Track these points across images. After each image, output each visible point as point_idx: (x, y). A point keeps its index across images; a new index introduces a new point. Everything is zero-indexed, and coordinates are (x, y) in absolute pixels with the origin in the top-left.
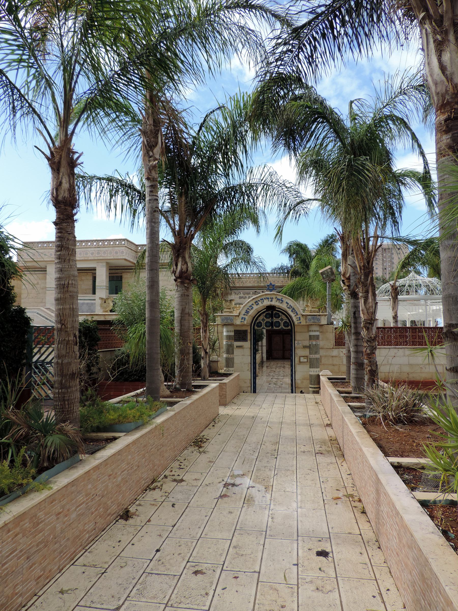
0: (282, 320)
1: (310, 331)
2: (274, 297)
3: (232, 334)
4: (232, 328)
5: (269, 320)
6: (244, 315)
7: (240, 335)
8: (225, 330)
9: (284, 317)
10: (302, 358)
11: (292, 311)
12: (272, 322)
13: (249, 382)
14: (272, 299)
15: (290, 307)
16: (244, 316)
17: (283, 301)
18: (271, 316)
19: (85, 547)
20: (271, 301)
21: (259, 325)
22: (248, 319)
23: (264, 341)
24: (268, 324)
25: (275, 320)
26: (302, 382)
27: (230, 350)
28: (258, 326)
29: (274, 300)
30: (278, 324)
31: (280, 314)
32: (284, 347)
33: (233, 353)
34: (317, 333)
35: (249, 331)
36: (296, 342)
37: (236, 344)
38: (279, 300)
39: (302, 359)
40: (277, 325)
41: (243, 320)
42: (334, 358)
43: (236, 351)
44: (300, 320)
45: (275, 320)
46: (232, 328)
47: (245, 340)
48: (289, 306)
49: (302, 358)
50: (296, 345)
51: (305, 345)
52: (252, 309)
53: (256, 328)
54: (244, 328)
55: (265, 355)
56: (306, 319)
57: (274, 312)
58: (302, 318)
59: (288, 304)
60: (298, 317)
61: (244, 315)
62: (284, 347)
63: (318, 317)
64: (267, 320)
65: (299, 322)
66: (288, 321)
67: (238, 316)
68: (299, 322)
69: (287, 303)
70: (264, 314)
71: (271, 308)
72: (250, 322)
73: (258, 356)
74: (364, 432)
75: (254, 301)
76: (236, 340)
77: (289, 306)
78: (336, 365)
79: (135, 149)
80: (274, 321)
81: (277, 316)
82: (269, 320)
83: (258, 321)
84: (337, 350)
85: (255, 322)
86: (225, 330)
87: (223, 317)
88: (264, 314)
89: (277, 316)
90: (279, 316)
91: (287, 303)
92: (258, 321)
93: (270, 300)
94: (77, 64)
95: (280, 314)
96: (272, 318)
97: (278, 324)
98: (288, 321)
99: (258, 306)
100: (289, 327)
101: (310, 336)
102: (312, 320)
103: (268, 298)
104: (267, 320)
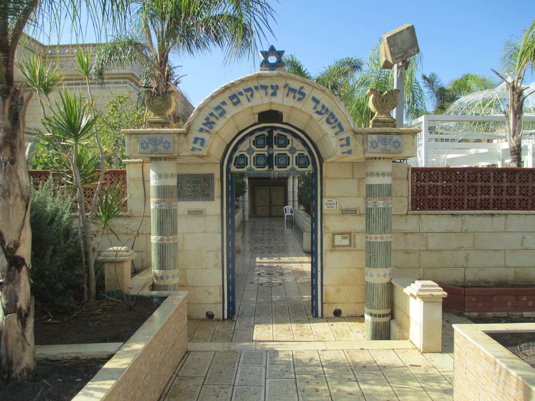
1: (372, 174)
2: (281, 83)
3: (173, 182)
5: (264, 151)
6: (201, 130)
7: (193, 186)
8: (152, 174)
9: (296, 144)
10: (338, 238)
11: (328, 121)
12: (271, 156)
13: (218, 291)
14: (275, 88)
15: (323, 111)
17: (303, 94)
18: (269, 141)
20: (274, 94)
21: (241, 161)
22: (215, 147)
23: (247, 195)
24: (262, 161)
25: (276, 150)
26: (338, 291)
27: (167, 222)
28: (238, 166)
29: (281, 93)
30: (285, 161)
31: (289, 137)
32: (270, 202)
33: (175, 232)
34: (387, 180)
35: (217, 176)
36: (325, 201)
37: (183, 207)
38: (293, 90)
39: (339, 240)
40: (283, 162)
41: (198, 146)
42: (409, 236)
43: (183, 225)
44: (348, 144)
45: (276, 150)
46: (171, 168)
47: (208, 196)
48: (319, 108)
49: (338, 238)
50: (325, 207)
51: (344, 206)
52: (221, 115)
53: (233, 169)
54: (205, 170)
55: (247, 213)
56: (364, 142)
57: (275, 133)
58: (353, 142)
60: (344, 136)
61: (201, 130)
62: (270, 202)
63: (395, 137)
65: (346, 149)
66: (306, 153)
67: (186, 134)
68: (346, 149)
69: (314, 99)
70: (253, 138)
71: (271, 116)
73: (238, 217)
75: (228, 94)
76: (181, 196)
77: (319, 108)
78: (414, 252)
79: (118, 10)
80: (276, 153)
81: (282, 142)
82: (264, 151)
83: (237, 154)
84: (415, 219)
86: (152, 174)
87: (145, 138)
88: (253, 138)
89: (282, 142)
90: (287, 142)
91: (314, 99)
92: (237, 154)
93: (270, 91)
95: (289, 137)
96: (271, 146)
99: (238, 109)
100: (310, 168)
101: (370, 188)
102: (381, 146)
103: (265, 88)
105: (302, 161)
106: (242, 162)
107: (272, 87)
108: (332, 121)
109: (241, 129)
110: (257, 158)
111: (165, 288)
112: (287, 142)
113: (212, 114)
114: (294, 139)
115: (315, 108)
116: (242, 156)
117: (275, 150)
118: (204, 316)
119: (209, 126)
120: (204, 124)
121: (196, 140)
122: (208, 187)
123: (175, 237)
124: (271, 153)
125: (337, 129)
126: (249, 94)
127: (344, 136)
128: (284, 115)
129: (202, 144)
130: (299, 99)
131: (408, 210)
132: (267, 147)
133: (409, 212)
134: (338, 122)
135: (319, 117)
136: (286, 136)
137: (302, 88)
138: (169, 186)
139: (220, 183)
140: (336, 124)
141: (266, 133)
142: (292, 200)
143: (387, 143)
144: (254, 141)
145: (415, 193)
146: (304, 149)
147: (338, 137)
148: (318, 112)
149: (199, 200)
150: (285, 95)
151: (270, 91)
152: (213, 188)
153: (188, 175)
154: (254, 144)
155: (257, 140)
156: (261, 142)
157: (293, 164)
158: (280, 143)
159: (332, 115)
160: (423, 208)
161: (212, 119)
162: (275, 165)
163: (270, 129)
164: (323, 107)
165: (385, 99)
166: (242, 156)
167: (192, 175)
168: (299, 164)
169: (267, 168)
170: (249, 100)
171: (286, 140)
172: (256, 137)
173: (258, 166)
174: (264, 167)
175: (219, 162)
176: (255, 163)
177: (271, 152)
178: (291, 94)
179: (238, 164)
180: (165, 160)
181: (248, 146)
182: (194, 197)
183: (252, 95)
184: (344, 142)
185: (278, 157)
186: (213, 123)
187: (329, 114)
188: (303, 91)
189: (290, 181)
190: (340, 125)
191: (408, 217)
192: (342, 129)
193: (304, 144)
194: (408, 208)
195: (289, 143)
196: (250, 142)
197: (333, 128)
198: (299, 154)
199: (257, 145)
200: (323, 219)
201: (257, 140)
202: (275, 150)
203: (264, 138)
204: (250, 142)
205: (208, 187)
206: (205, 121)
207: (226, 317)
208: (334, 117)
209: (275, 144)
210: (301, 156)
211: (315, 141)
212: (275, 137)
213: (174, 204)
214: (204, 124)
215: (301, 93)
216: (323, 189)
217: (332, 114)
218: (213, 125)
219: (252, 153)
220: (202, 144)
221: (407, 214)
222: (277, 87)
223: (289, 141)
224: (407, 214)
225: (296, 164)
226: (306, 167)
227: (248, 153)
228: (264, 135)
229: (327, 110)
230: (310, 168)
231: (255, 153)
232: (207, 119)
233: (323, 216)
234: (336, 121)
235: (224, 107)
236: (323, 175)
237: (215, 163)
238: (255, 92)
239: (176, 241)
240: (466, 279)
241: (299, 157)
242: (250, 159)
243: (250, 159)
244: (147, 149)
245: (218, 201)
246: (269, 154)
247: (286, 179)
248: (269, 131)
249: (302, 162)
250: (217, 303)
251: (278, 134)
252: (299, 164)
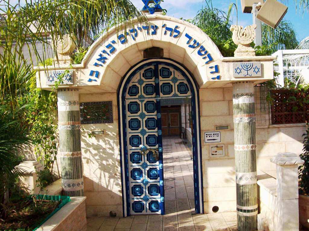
0: (175, 80)
4: (75, 97)
5: (152, 81)
9: (178, 75)
11: (199, 53)
12: (157, 85)
16: (95, 69)
18: (155, 73)
19: (86, 207)
20: (154, 33)
24: (150, 90)
25: (162, 81)
31: (172, 70)
35: (115, 103)
38: (170, 29)
41: (93, 78)
45: (162, 81)
47: (109, 120)
48: (192, 43)
54: (105, 99)
57: (160, 67)
59: (190, 38)
61: (96, 65)
64: (147, 81)
65: (216, 75)
66: (186, 82)
68: (216, 75)
69: (187, 35)
70: (142, 71)
72: (116, 87)
74: (258, 219)
76: (86, 121)
77: (192, 43)
81: (166, 73)
82: (152, 81)
83: (130, 85)
85: (126, 86)
88: (142, 71)
89: (166, 73)
90: (170, 74)
91: (187, 35)
92: (130, 85)
94: (11, 11)
95: (172, 70)
96: (157, 77)
97: (168, 89)
98: (186, 82)
99: (127, 45)
100: (189, 93)
104: (147, 81)
105: (183, 88)
106: (134, 91)
107: (153, 27)
108: (203, 53)
109: (133, 64)
110: (146, 87)
111: (72, 194)
112: (170, 74)
113: (104, 52)
114: (176, 71)
115: (188, 43)
116: (135, 86)
117: (161, 81)
118: (109, 214)
119: (103, 60)
120: (98, 60)
121: (92, 73)
122: (107, 112)
123: (79, 152)
124: (157, 82)
125: (208, 59)
126: (133, 34)
127: (213, 64)
128: (164, 51)
129: (97, 76)
130: (175, 37)
131: (269, 125)
132: (154, 78)
133: (270, 126)
134: (207, 54)
135: (192, 49)
136: (169, 69)
137: (177, 27)
138: (74, 111)
139: (117, 109)
140: (206, 56)
141: (152, 67)
142: (184, 122)
143: (248, 69)
144: (143, 74)
145: (274, 111)
146: (184, 79)
147: (207, 65)
148: (190, 46)
149: (101, 123)
150: (164, 32)
151: (152, 30)
152: (112, 113)
153: (92, 103)
154: (143, 76)
155: (146, 73)
156: (149, 74)
157: (175, 90)
158: (164, 75)
159: (203, 48)
160: (218, 70)
161: (105, 55)
162: (161, 92)
163: (155, 64)
164: (195, 42)
165: (244, 34)
166: (135, 86)
167: (95, 102)
168: (180, 91)
169: (154, 95)
170: (134, 39)
171: (169, 72)
172: (145, 71)
173: (147, 93)
174: (152, 95)
175: (116, 91)
176: (145, 92)
177: (157, 82)
178: (169, 33)
179: (131, 93)
180: (68, 90)
181: (139, 78)
182: (96, 120)
183: (136, 35)
184: (214, 70)
185: (163, 86)
186: (105, 58)
187: (199, 48)
188: (178, 29)
189: (183, 109)
190: (209, 56)
191: (269, 130)
192: (211, 60)
193: (184, 74)
194: (269, 122)
195: (171, 75)
196: (140, 74)
197: (204, 58)
198: (180, 83)
199: (146, 77)
200: (202, 134)
201: (146, 73)
202: (161, 81)
203: (151, 72)
204: (140, 74)
205: (107, 112)
206: (99, 57)
207: (126, 215)
208: (204, 49)
209: (160, 75)
210: (181, 84)
211: (180, 62)
212: (160, 70)
213: (77, 125)
214: (98, 60)
215: (176, 31)
216: (201, 110)
217: (202, 47)
218: (106, 60)
219: (143, 84)
220: (97, 76)
221: (269, 128)
222: (156, 27)
223: (171, 72)
224: (269, 128)
225: (178, 91)
226: (186, 93)
227: (139, 84)
228: (151, 68)
229: (198, 44)
230: (189, 93)
231: (145, 84)
232: (101, 55)
233: (201, 132)
234: (206, 52)
235: (115, 46)
236: (200, 99)
237: (113, 93)
238: (139, 31)
239: (79, 156)
240: (117, 71)
241: (180, 86)
242: (141, 88)
243: (141, 88)
244: (53, 82)
245: (116, 123)
246: (155, 83)
247: (179, 107)
248: (155, 66)
249: (183, 89)
250: (118, 204)
251: (163, 68)
252: (180, 91)
